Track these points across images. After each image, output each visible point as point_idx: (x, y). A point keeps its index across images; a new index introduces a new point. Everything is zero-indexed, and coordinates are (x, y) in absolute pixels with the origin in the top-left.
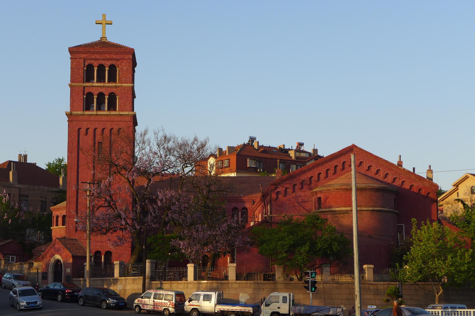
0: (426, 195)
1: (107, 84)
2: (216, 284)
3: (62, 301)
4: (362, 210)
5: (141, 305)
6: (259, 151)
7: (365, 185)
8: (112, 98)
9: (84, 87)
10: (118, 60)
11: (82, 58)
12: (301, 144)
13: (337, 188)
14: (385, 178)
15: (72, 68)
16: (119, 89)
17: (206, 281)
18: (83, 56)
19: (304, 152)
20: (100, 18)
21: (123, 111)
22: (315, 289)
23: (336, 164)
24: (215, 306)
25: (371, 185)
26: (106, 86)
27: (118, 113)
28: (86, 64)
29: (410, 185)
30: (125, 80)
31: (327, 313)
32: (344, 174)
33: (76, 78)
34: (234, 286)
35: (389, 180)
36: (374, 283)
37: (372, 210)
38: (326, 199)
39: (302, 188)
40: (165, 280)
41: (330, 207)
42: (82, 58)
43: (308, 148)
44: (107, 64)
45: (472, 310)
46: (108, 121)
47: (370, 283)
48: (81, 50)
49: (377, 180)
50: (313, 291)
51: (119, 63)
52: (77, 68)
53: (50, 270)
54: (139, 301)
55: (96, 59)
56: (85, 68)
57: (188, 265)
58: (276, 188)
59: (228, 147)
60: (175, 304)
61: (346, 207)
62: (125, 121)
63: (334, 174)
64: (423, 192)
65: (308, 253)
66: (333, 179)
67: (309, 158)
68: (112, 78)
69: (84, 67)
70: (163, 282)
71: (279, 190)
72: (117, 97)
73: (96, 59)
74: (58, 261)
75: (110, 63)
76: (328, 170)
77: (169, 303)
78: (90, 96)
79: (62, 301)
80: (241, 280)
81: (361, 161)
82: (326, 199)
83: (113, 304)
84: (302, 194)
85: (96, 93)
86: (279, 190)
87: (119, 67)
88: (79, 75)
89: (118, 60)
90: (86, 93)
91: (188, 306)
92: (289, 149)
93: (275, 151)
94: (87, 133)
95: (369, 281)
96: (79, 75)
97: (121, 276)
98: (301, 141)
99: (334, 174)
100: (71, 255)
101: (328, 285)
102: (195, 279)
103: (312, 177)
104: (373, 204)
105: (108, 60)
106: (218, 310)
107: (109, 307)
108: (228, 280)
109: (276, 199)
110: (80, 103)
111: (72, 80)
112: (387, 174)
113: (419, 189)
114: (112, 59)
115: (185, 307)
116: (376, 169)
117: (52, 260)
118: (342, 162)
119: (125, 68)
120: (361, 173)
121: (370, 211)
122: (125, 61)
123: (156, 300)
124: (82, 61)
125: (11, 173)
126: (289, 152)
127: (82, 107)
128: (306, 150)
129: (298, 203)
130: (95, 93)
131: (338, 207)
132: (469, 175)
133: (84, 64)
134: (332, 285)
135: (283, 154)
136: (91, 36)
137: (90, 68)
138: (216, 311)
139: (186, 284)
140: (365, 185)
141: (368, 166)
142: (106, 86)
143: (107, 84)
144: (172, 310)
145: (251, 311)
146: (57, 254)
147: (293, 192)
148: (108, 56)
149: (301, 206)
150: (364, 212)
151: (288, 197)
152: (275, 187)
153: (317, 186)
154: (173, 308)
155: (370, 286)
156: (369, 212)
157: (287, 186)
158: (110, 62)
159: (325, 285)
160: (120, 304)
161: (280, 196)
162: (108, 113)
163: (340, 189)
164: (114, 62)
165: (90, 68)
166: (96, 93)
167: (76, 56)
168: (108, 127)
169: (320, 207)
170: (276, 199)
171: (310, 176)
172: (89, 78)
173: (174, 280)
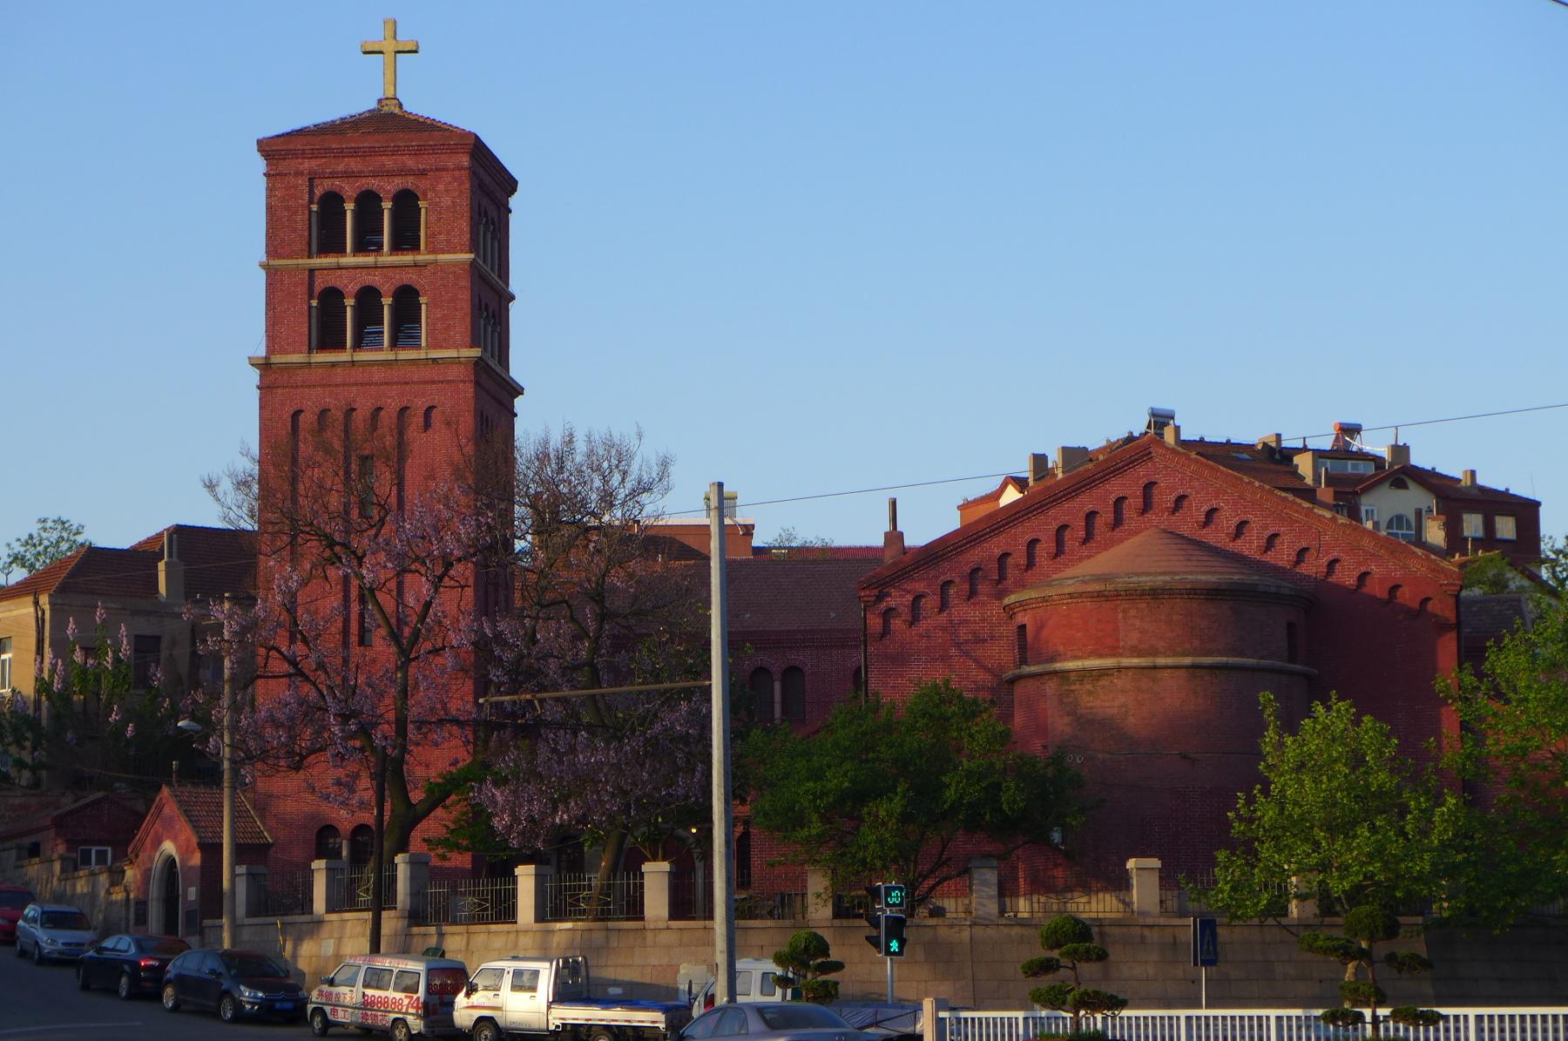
0: (1415, 605)
1: (387, 258)
2: (603, 933)
3: (131, 997)
4: (1155, 667)
5: (328, 1009)
7: (1167, 578)
8: (407, 299)
9: (311, 271)
10: (423, 173)
11: (302, 174)
12: (1350, 430)
13: (1071, 590)
14: (1267, 549)
15: (269, 208)
16: (426, 272)
17: (569, 925)
18: (307, 165)
19: (1362, 456)
20: (376, 36)
21: (441, 347)
22: (901, 946)
23: (1089, 507)
24: (549, 1008)
25: (1203, 578)
26: (350, 266)
27: (423, 356)
28: (318, 192)
29: (1356, 574)
30: (448, 241)
31: (909, 1030)
33: (283, 240)
34: (664, 938)
35: (1282, 555)
36: (1162, 921)
37: (1194, 667)
38: (1040, 628)
39: (973, 593)
40: (454, 923)
41: (1052, 660)
42: (302, 174)
43: (1375, 443)
44: (388, 188)
45: (1562, 1011)
46: (433, 382)
47: (1149, 921)
48: (298, 145)
49: (1238, 558)
50: (894, 953)
51: (423, 184)
52: (287, 208)
53: (155, 891)
54: (321, 993)
55: (348, 175)
56: (315, 208)
57: (647, 867)
58: (880, 598)
60: (426, 1005)
61: (1101, 656)
62: (448, 382)
63: (1085, 541)
64: (1406, 596)
65: (905, 818)
66: (1081, 559)
67: (1370, 477)
68: (406, 239)
69: (311, 202)
70: (446, 929)
71: (890, 602)
72: (422, 300)
73: (348, 175)
74: (170, 862)
75: (396, 184)
76: (1063, 528)
77: (406, 1001)
78: (332, 297)
79: (131, 997)
80: (693, 919)
82: (1040, 628)
83: (253, 1004)
84: (970, 612)
85: (350, 288)
86: (890, 602)
87: (425, 199)
88: (295, 230)
89: (423, 173)
90: (317, 289)
91: (465, 1009)
92: (1298, 451)
93: (1245, 456)
94: (427, 425)
95: (1143, 914)
96: (295, 230)
97: (334, 911)
98: (1350, 419)
99: (1085, 541)
100: (195, 840)
101: (991, 932)
102: (540, 917)
103: (1006, 555)
104: (1196, 643)
105: (390, 174)
106: (558, 1022)
107: (241, 1017)
108: (642, 919)
109: (883, 635)
110: (300, 325)
112: (1276, 535)
115: (456, 1014)
116: (1236, 521)
117: (158, 861)
118: (1113, 498)
119: (447, 201)
120: (1182, 537)
121: (1187, 667)
122: (447, 177)
123: (370, 992)
124: (302, 182)
125: (161, 566)
126: (1296, 460)
128: (1367, 448)
129: (958, 645)
130: (350, 288)
131: (1076, 658)
134: (1005, 930)
135: (1272, 466)
136: (353, 96)
137: (332, 203)
138: (552, 1027)
139: (512, 936)
140: (1167, 578)
141: (1205, 508)
142: (350, 266)
143: (387, 258)
144: (416, 1025)
145: (662, 1026)
146: (169, 838)
147: (941, 610)
148: (389, 163)
149: (967, 654)
150: (1166, 673)
151: (924, 625)
152: (876, 592)
153: (1022, 586)
154: (418, 1016)
155: (1147, 932)
156: (1181, 673)
157: (920, 587)
159: (978, 931)
160: (278, 1005)
161: (897, 624)
162: (391, 356)
163: (1081, 595)
164: (409, 183)
166: (350, 288)
167: (283, 166)
168: (392, 404)
169: (1023, 661)
170: (883, 635)
171: (997, 552)
172: (330, 242)
173: (482, 920)
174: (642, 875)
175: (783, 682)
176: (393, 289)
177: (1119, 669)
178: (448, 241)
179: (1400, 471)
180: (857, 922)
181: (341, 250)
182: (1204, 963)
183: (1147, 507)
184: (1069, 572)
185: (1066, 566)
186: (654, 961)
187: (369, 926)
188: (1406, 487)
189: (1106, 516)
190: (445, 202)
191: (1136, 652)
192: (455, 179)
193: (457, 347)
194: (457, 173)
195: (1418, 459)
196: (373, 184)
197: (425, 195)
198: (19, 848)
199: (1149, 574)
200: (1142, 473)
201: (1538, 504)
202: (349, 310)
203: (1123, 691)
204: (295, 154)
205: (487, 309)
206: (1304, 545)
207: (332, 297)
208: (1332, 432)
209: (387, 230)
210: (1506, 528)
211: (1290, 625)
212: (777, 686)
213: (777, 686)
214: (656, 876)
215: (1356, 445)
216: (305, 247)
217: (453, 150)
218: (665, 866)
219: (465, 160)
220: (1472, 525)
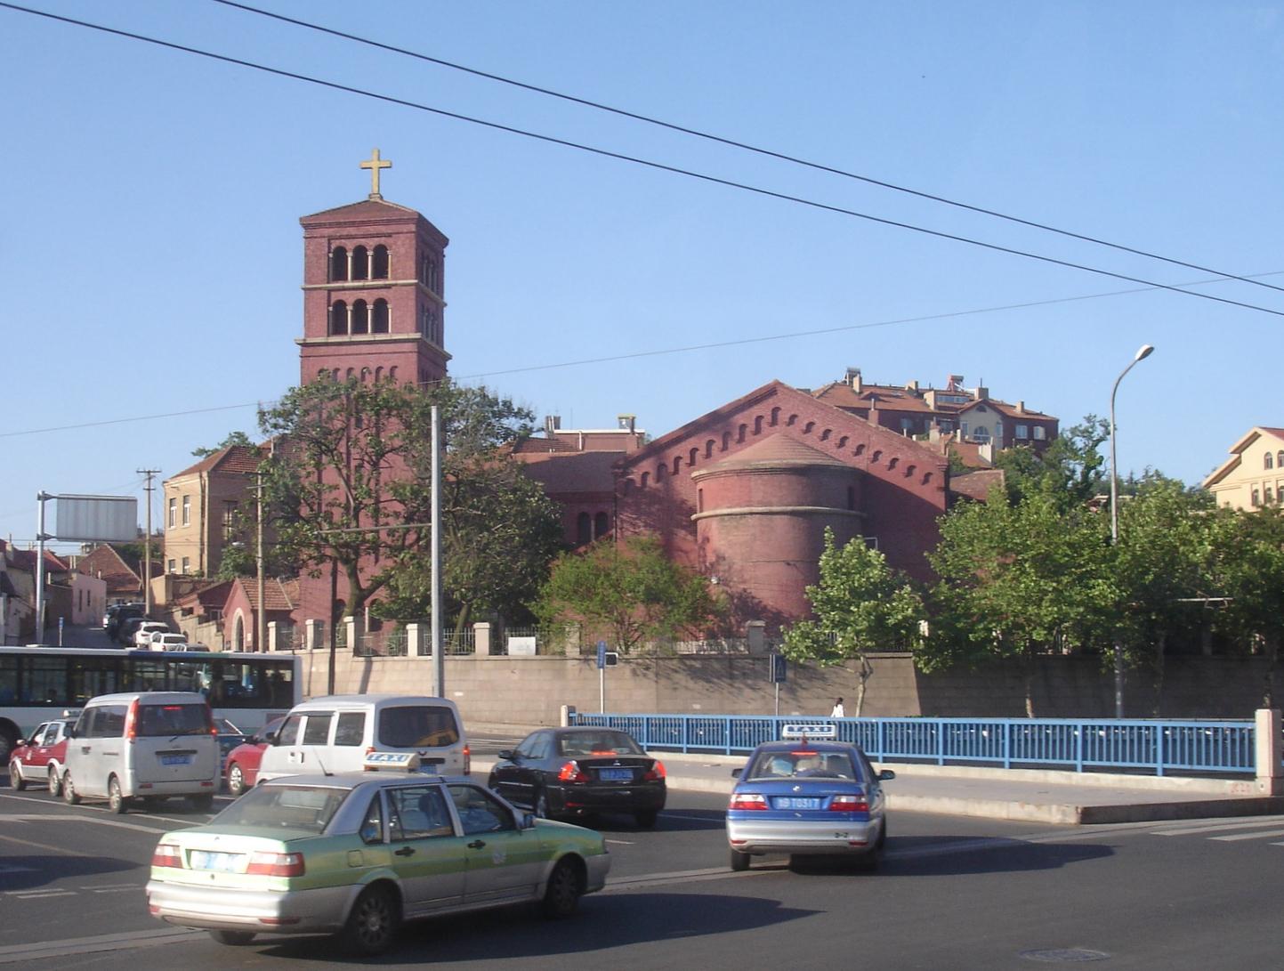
6: (862, 396)
18: (327, 232)
19: (964, 394)
26: (350, 289)
28: (333, 247)
29: (890, 459)
30: (403, 273)
32: (759, 440)
34: (487, 665)
44: (371, 244)
52: (316, 256)
56: (331, 255)
57: (477, 625)
59: (987, 389)
68: (380, 272)
72: (389, 306)
81: (793, 413)
89: (390, 235)
90: (332, 302)
97: (280, 650)
105: (372, 236)
110: (322, 322)
111: (307, 280)
113: (907, 466)
114: (378, 236)
119: (402, 250)
124: (325, 241)
126: (925, 396)
127: (326, 329)
132: (1260, 431)
133: (329, 248)
136: (352, 193)
137: (340, 253)
148: (372, 229)
158: (376, 239)
164: (382, 241)
165: (340, 253)
172: (339, 274)
174: (407, 631)
175: (596, 520)
176: (374, 300)
177: (751, 514)
178: (403, 273)
179: (985, 403)
180: (906, 655)
181: (345, 279)
182: (777, 680)
183: (774, 422)
184: (729, 458)
185: (728, 455)
186: (481, 679)
187: (329, 655)
188: (985, 411)
189: (751, 427)
190: (402, 253)
191: (761, 504)
192: (407, 238)
193: (408, 333)
194: (409, 235)
195: (994, 396)
196: (362, 242)
197: (391, 247)
198: (183, 610)
199: (768, 460)
200: (771, 403)
201: (1058, 421)
202: (369, 312)
203: (753, 526)
204: (320, 226)
205: (428, 310)
206: (861, 443)
207: (340, 305)
208: (948, 380)
209: (376, 266)
210: (1040, 433)
211: (850, 489)
212: (593, 523)
213: (593, 523)
214: (412, 630)
215: (960, 387)
216: (326, 278)
217: (407, 221)
218: (487, 625)
219: (413, 227)
220: (1022, 432)
